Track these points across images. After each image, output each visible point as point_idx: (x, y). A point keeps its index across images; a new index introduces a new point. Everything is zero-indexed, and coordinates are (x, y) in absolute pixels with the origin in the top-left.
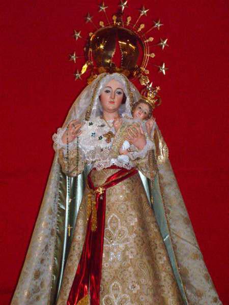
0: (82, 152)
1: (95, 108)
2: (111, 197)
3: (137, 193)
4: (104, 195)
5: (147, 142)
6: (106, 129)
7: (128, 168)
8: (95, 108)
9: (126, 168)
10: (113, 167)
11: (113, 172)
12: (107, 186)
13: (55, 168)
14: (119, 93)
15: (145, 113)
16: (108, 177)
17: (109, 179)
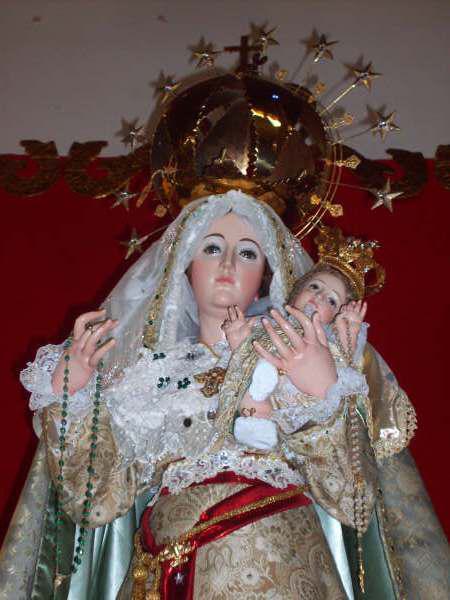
0: (124, 437)
1: (174, 307)
2: (213, 574)
3: (305, 567)
4: (188, 568)
5: (341, 373)
6: (207, 363)
7: (277, 484)
8: (174, 307)
9: (269, 480)
10: (226, 477)
11: (222, 492)
12: (202, 538)
13: (37, 485)
14: (250, 254)
15: (333, 302)
16: (205, 508)
17: (211, 513)
